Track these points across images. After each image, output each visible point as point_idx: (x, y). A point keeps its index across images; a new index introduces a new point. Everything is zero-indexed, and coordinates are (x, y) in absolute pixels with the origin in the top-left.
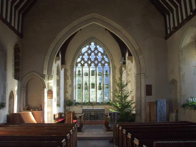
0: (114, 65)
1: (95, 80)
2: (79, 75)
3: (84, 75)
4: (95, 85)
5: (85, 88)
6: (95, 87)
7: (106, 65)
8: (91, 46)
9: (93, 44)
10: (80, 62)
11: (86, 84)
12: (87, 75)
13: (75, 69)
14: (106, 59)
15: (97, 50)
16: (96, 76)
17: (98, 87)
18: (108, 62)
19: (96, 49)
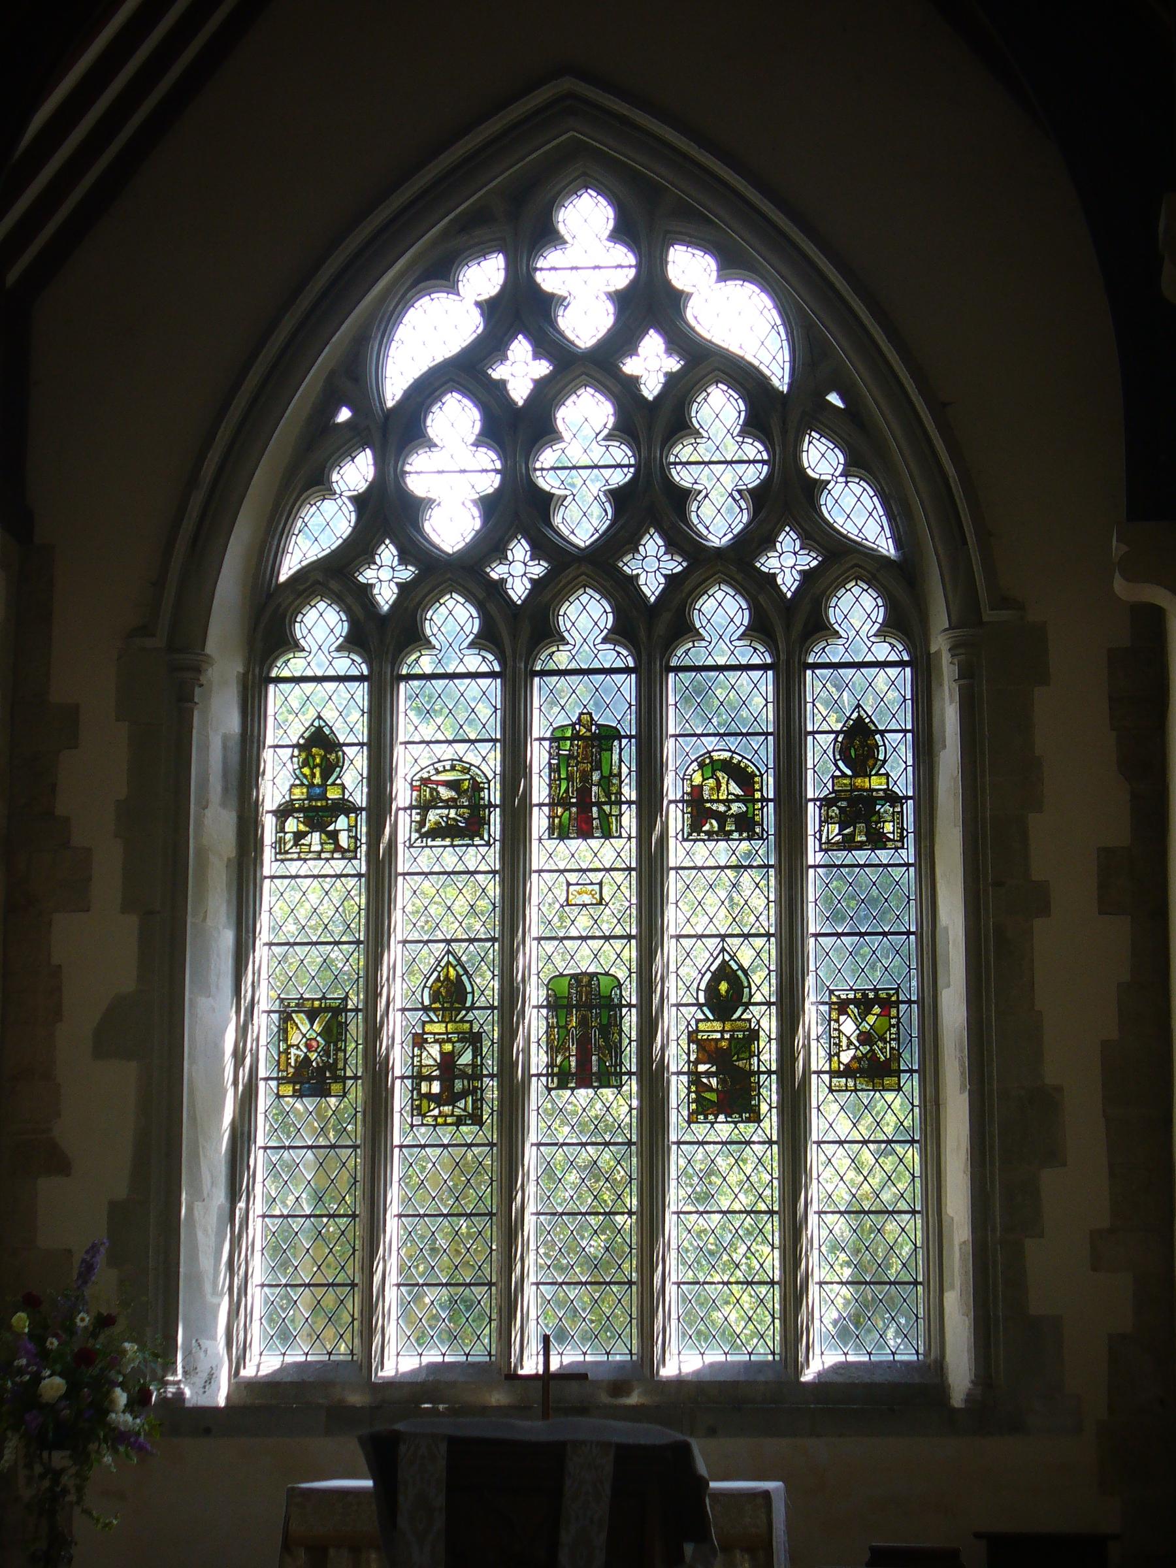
0: (1003, 602)
1: (542, 894)
2: (318, 812)
3: (404, 825)
4: (630, 1021)
5: (419, 1077)
6: (631, 1062)
7: (857, 611)
8: (551, 272)
9: (586, 217)
10: (336, 576)
12: (468, 829)
13: (220, 718)
14: (856, 512)
15: (682, 340)
18: (886, 547)
19: (649, 304)
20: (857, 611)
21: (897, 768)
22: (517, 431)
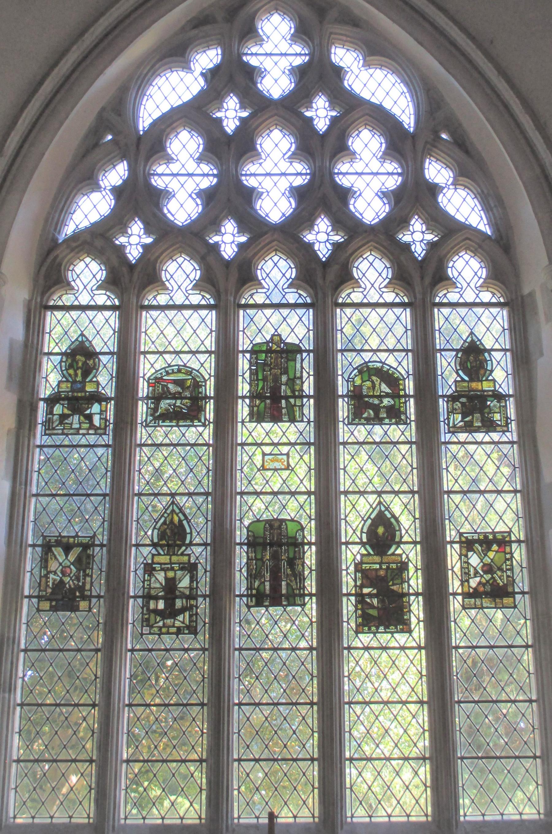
2: (77, 400)
4: (310, 557)
7: (467, 270)
10: (99, 240)
11: (173, 535)
12: (191, 414)
14: (462, 205)
16: (113, 626)
17: (348, 581)
20: (467, 270)
21: (501, 375)
22: (230, 150)
